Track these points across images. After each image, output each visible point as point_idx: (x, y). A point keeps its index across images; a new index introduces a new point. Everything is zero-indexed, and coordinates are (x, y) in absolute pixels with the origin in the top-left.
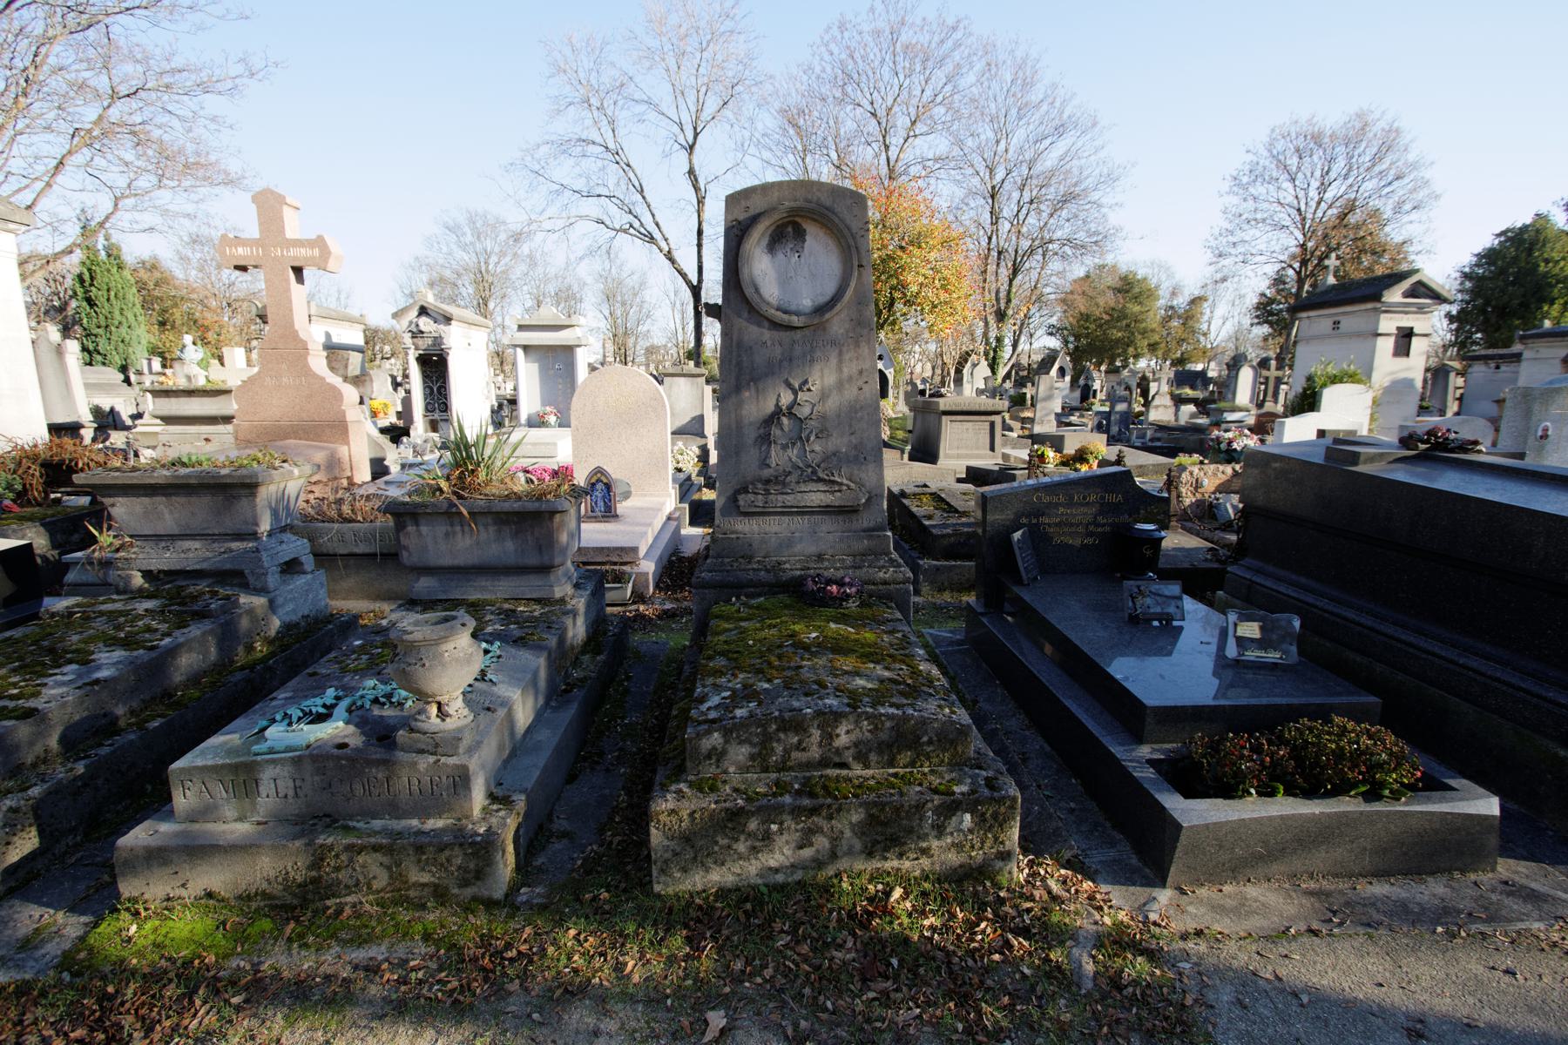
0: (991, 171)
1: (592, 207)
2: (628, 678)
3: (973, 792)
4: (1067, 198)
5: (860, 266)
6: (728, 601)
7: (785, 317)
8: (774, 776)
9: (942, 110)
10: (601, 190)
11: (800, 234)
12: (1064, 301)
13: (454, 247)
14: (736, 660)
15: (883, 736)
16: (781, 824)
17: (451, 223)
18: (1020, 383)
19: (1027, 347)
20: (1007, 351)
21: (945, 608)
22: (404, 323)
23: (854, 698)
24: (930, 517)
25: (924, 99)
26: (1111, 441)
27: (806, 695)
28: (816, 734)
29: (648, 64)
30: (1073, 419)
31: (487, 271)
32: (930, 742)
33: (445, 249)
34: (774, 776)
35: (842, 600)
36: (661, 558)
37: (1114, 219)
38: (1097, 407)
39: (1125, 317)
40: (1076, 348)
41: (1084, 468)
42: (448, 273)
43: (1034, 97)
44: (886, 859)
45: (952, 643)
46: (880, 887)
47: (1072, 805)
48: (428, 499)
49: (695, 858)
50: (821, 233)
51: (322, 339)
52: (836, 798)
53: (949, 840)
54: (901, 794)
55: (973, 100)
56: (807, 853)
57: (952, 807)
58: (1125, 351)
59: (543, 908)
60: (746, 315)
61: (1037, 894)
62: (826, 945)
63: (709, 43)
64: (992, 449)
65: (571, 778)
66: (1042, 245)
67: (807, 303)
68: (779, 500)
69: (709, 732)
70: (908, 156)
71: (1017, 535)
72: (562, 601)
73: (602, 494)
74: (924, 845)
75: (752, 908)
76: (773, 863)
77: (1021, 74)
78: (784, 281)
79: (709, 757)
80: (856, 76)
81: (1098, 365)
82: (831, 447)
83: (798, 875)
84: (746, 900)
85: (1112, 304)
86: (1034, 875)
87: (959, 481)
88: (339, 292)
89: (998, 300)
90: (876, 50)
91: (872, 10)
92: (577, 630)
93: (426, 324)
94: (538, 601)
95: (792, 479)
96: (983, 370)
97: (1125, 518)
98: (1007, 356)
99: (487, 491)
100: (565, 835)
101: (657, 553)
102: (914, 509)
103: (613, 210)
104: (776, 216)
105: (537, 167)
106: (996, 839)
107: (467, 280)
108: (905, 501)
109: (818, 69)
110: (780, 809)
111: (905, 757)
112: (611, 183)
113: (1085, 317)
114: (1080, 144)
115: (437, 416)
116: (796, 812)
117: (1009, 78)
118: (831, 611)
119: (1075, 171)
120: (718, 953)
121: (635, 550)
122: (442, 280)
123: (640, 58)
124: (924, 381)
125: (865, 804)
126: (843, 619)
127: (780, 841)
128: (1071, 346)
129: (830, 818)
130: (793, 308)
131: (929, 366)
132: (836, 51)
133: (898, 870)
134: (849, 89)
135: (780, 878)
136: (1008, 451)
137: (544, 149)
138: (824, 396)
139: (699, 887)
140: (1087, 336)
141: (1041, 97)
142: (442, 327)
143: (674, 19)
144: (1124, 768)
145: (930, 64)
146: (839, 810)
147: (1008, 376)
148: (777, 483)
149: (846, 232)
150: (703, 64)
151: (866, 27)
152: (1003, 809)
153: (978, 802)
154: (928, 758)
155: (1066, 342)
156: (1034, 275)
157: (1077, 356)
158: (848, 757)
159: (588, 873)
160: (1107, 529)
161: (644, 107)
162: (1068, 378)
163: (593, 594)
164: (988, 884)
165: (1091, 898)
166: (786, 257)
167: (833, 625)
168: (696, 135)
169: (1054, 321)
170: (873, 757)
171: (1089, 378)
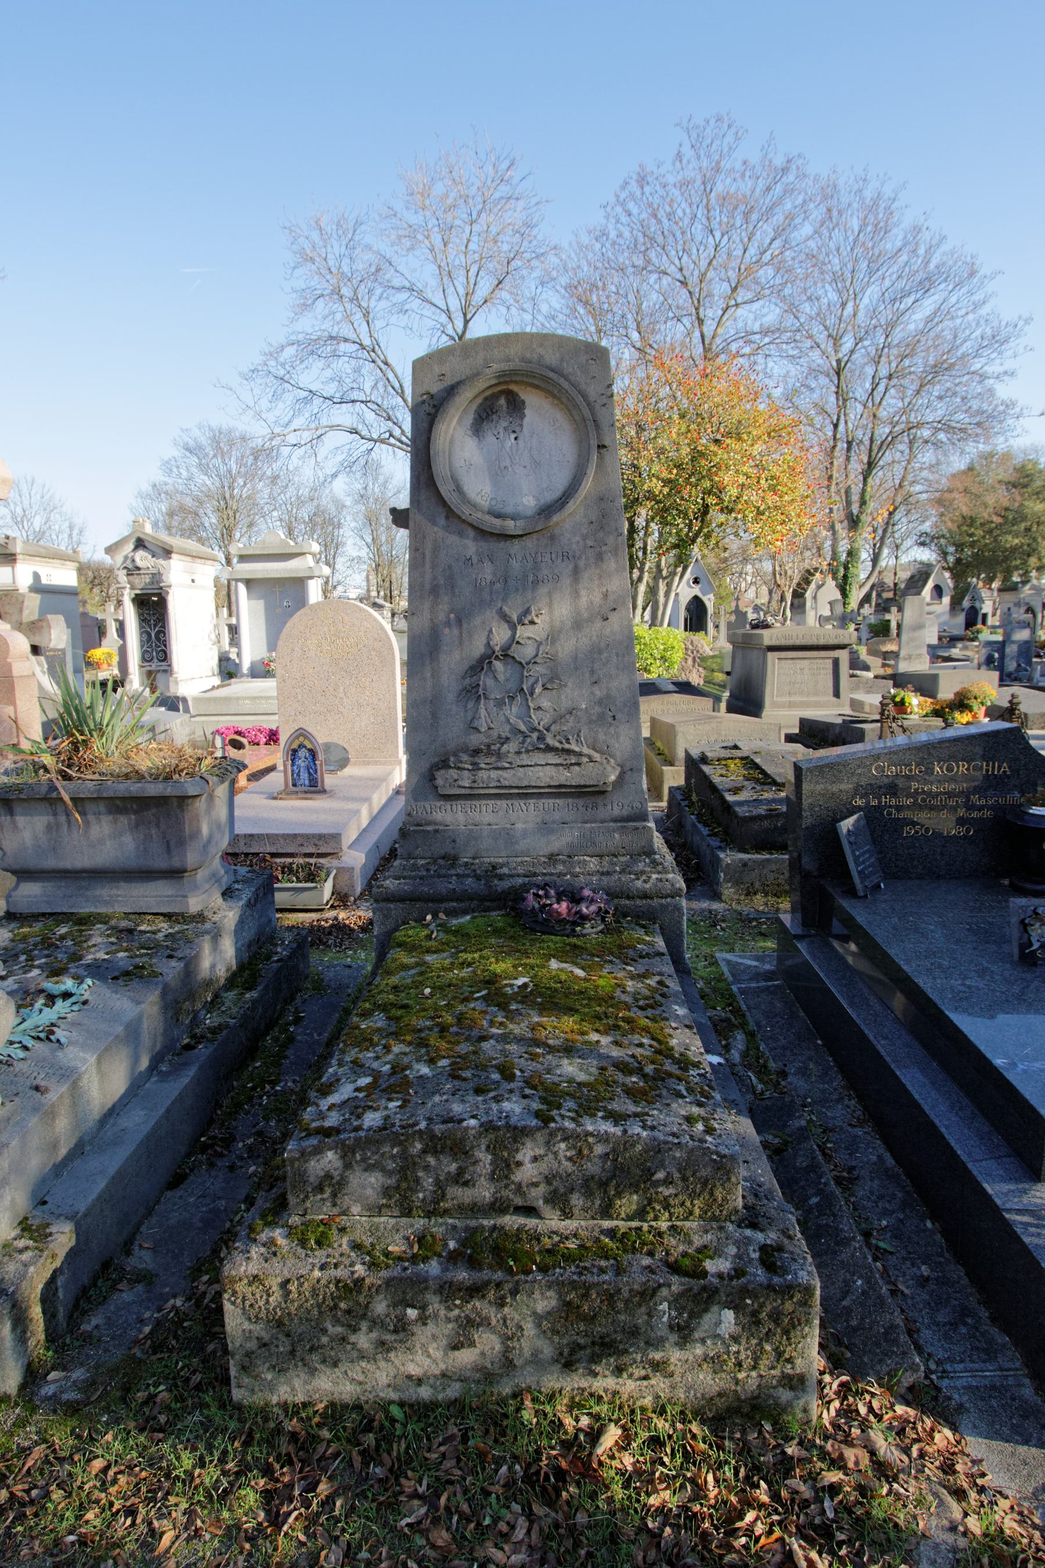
1: (344, 415)
2: (297, 1021)
3: (738, 1273)
4: (937, 370)
6: (420, 920)
7: (497, 522)
8: (420, 1223)
9: (770, 271)
10: (355, 395)
11: (516, 406)
12: (940, 502)
13: (194, 470)
14: (398, 1019)
15: (593, 1168)
16: (423, 1308)
17: (191, 443)
18: (883, 607)
19: (892, 562)
20: (862, 571)
21: (747, 922)
22: (119, 559)
23: (550, 1097)
24: (736, 791)
26: (1006, 679)
27: (478, 1091)
28: (485, 1158)
29: (408, 244)
30: (955, 652)
31: (232, 497)
32: (668, 1182)
34: (420, 1223)
35: (575, 924)
36: (377, 846)
37: (1003, 391)
38: (986, 635)
39: (1024, 518)
40: (958, 561)
41: (965, 718)
42: (188, 501)
43: (892, 243)
44: (595, 1375)
45: (757, 976)
46: (585, 1421)
47: (925, 1270)
48: (28, 778)
49: (293, 1352)
51: (29, 581)
52: (509, 1271)
53: (699, 1351)
54: (619, 1271)
55: (811, 256)
56: (466, 1357)
57: (701, 1297)
58: (1025, 563)
59: (73, 1409)
60: (442, 521)
61: (850, 1455)
62: (482, 1531)
64: (837, 694)
65: (176, 1180)
66: (908, 432)
67: (528, 502)
68: (488, 776)
69: (318, 1151)
70: (729, 329)
71: (847, 825)
72: (200, 918)
73: (309, 767)
74: (657, 1356)
75: (372, 1444)
76: (413, 1370)
77: (871, 218)
78: (497, 472)
79: (320, 1189)
80: (660, 239)
81: (990, 580)
82: (565, 704)
83: (454, 1391)
84: (368, 1428)
85: (1006, 503)
86: (848, 1413)
87: (790, 739)
88: (71, 528)
89: (849, 503)
91: (679, 156)
92: (218, 957)
93: (142, 559)
94: (168, 916)
95: (511, 747)
96: (831, 591)
97: (1015, 797)
98: (863, 576)
99: (102, 767)
100: (145, 1278)
101: (373, 838)
102: (716, 780)
103: (370, 416)
104: (481, 384)
105: (282, 372)
106: (779, 1354)
107: (209, 507)
108: (706, 768)
109: (613, 235)
110: (420, 1283)
111: (628, 1203)
112: (367, 387)
114: (953, 300)
115: (154, 666)
116: (448, 1291)
117: (855, 224)
118: (554, 941)
119: (948, 335)
120: (306, 1530)
121: (336, 837)
122: (182, 508)
123: (399, 237)
124: (757, 609)
125: (559, 1285)
126: (573, 953)
127: (423, 1334)
128: (951, 559)
129: (501, 1303)
130: (509, 510)
131: (764, 590)
132: (635, 211)
133: (615, 1393)
134: (652, 255)
135: (425, 1393)
136: (860, 696)
137: (290, 351)
138: (553, 637)
139: (300, 1398)
140: (972, 545)
141: (899, 244)
142: (161, 561)
143: (439, 189)
144: (1007, 1225)
145: (754, 216)
146: (514, 1292)
147: (866, 599)
148: (489, 753)
149: (579, 399)
150: (475, 239)
151: (671, 179)
152: (789, 1306)
153: (745, 1292)
154: (667, 1207)
155: (944, 554)
156: (898, 470)
157: (960, 570)
158: (537, 1196)
159: (156, 1349)
160: (987, 814)
161: (404, 296)
162: (946, 600)
163: (250, 905)
164: (768, 1427)
165: (948, 1468)
166: (500, 438)
167: (554, 964)
168: (466, 322)
169: (927, 527)
170: (577, 1200)
171: (976, 598)
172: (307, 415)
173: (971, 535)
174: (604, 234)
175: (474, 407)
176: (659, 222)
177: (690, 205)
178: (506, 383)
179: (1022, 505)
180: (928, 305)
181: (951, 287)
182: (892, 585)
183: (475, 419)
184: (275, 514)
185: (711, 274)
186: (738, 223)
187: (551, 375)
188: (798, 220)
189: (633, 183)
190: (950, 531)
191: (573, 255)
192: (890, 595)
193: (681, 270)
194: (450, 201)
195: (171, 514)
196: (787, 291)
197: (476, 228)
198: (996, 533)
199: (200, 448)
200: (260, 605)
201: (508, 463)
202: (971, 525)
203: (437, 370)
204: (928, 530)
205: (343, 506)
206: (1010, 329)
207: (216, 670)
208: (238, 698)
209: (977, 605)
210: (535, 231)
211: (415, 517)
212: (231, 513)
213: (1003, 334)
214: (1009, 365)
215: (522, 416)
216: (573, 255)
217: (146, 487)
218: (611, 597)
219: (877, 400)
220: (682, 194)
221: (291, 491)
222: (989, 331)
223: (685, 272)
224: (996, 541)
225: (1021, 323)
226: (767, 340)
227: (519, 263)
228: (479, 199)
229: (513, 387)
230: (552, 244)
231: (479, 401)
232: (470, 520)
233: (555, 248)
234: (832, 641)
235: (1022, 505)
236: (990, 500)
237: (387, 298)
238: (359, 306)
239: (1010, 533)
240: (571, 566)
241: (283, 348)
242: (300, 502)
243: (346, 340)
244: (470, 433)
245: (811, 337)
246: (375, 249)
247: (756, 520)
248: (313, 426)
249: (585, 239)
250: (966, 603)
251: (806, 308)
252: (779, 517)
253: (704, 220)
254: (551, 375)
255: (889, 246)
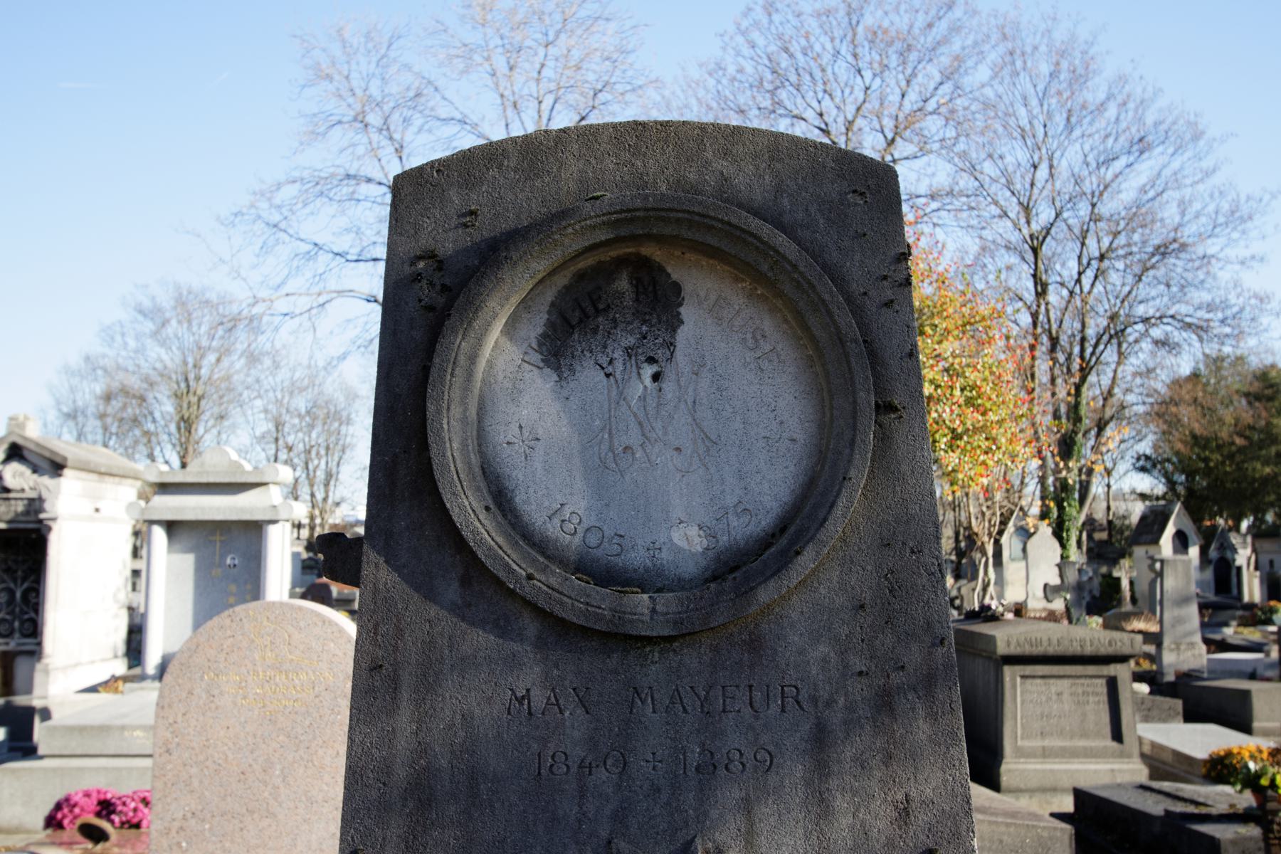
0: (1027, 209)
4: (1162, 251)
5: (885, 407)
7: (603, 598)
11: (659, 303)
17: (147, 304)
25: (907, 106)
29: (461, 66)
31: (198, 378)
33: (132, 344)
40: (1191, 492)
42: (134, 383)
43: (1095, 92)
50: (736, 298)
60: (452, 591)
63: (558, 33)
64: (1117, 736)
67: (685, 540)
77: (1064, 65)
78: (605, 459)
80: (793, 78)
90: (825, 40)
104: (570, 242)
105: (276, 218)
109: (731, 70)
113: (1196, 439)
117: (1045, 69)
122: (125, 391)
123: (450, 58)
130: (636, 558)
132: (761, 42)
134: (783, 95)
141: (1101, 96)
142: (46, 480)
145: (913, 56)
149: (827, 289)
150: (550, 64)
155: (1171, 484)
157: (1196, 506)
162: (1194, 551)
166: (610, 384)
169: (1145, 447)
172: (309, 275)
173: (1206, 460)
174: (720, 67)
175: (549, 295)
176: (791, 56)
177: (832, 40)
178: (633, 238)
179: (1268, 424)
180: (1145, 170)
181: (1171, 150)
182: (1105, 522)
183: (550, 324)
184: (258, 403)
185: (860, 122)
186: (893, 64)
187: (755, 224)
188: (970, 63)
189: (759, 9)
190: (1177, 453)
191: (679, 92)
192: (1103, 536)
193: (821, 115)
194: (519, 17)
195: (108, 397)
196: (961, 147)
197: (552, 51)
198: (1238, 458)
199: (160, 310)
200: (187, 562)
201: (634, 438)
202: (1204, 448)
203: (455, 198)
204: (1148, 452)
205: (356, 396)
206: (1253, 204)
207: (121, 648)
208: (123, 728)
209: (1229, 554)
210: (631, 58)
211: (374, 566)
212: (194, 400)
213: (1245, 210)
214: (1257, 248)
215: (675, 323)
216: (679, 92)
217: (75, 361)
218: (921, 819)
219: (1086, 288)
220: (821, 26)
221: (283, 375)
222: (1225, 206)
223: (825, 117)
224: (1239, 468)
225: (1267, 197)
226: (934, 205)
227: (609, 97)
228: (558, 17)
229: (652, 251)
230: (653, 77)
231: (562, 280)
232: (527, 590)
233: (656, 81)
234: (1104, 651)
235: (1268, 424)
236: (1228, 415)
237: (430, 131)
238: (391, 138)
239: (1258, 458)
240: (806, 727)
241: (279, 186)
242: (294, 389)
243: (369, 180)
244: (536, 358)
245: (996, 203)
246: (416, 69)
247: (951, 447)
248: (315, 290)
249: (695, 73)
250: (1213, 553)
251: (989, 168)
252: (984, 444)
253: (850, 59)
254: (755, 224)
255: (1089, 97)
